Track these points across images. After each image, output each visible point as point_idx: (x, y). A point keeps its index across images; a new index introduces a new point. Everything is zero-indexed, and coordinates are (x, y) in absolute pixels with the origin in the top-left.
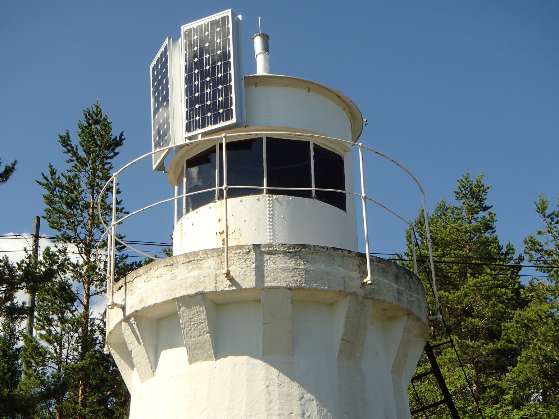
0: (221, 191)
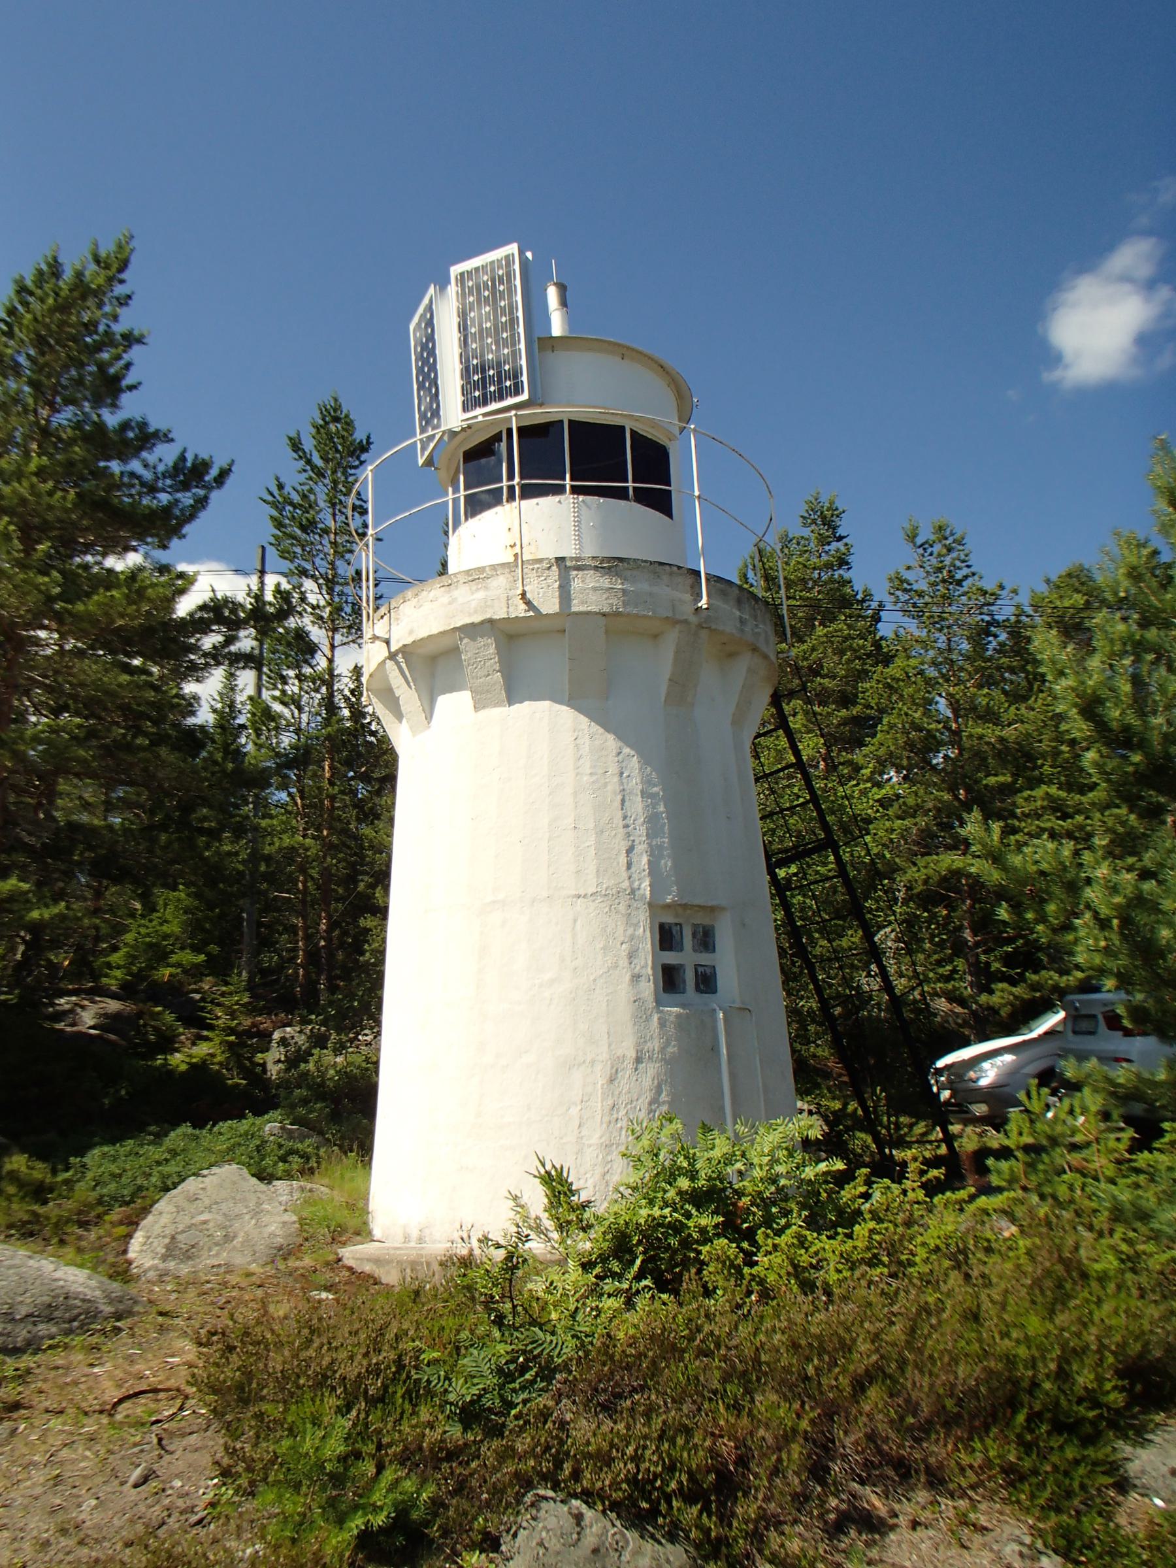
0: (511, 489)
